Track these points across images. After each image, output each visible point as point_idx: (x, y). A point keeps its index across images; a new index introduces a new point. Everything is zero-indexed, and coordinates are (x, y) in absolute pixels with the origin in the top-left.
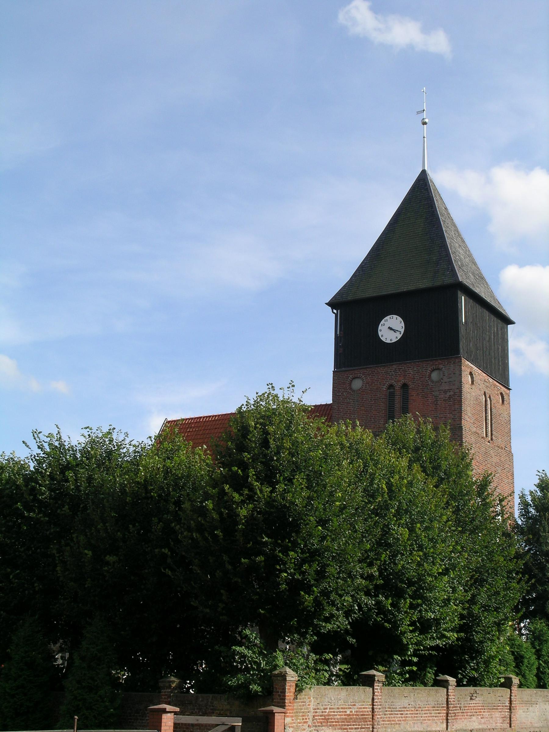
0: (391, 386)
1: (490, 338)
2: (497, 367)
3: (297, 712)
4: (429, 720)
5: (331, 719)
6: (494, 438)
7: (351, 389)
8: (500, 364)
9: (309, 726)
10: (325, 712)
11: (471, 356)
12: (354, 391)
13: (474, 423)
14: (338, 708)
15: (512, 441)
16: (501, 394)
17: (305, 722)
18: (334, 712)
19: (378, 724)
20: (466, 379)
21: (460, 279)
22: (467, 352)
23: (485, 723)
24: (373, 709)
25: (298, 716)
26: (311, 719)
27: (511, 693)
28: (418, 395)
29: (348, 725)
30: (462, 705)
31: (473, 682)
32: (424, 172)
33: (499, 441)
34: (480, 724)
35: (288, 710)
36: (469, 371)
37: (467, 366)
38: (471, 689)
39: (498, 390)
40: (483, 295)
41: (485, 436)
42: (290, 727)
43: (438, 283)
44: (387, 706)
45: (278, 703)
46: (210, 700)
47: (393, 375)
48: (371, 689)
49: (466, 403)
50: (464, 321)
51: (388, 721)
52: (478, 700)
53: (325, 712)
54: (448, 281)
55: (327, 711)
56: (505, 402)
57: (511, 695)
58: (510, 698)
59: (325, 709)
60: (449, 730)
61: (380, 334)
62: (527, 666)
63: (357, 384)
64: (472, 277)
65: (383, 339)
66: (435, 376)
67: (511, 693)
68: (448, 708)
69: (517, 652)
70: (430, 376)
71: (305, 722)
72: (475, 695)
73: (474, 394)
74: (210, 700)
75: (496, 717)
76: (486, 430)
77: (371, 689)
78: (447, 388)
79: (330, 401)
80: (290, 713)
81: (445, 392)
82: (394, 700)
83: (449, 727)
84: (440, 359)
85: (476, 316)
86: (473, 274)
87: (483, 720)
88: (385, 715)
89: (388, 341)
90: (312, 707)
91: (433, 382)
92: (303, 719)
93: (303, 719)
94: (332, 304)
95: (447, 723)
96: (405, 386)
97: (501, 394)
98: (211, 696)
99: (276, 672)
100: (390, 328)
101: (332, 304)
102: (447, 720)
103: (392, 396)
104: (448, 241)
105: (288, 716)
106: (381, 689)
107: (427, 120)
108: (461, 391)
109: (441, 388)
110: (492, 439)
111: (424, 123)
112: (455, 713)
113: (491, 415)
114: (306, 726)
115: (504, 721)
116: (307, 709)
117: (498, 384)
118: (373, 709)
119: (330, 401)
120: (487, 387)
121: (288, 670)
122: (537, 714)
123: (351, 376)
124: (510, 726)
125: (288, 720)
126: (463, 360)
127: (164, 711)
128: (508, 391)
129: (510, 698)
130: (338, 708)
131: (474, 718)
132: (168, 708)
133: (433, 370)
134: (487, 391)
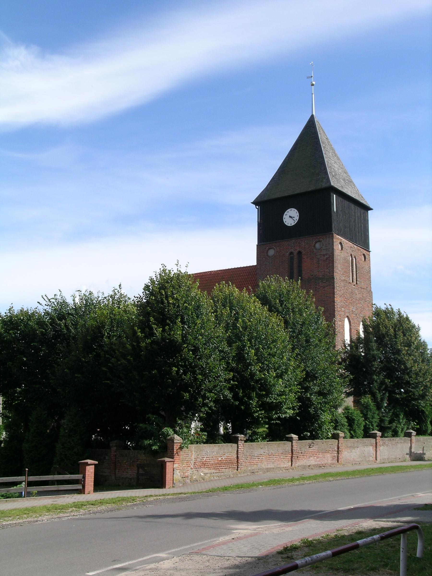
0: (291, 253)
1: (355, 220)
2: (361, 238)
3: (183, 461)
4: (279, 461)
5: (208, 463)
6: (358, 282)
7: (267, 255)
8: (363, 235)
9: (191, 468)
10: (203, 460)
11: (341, 232)
12: (269, 257)
13: (343, 274)
14: (213, 457)
15: (371, 284)
16: (364, 255)
17: (188, 466)
18: (209, 459)
19: (241, 465)
20: (337, 247)
21: (332, 184)
22: (337, 230)
23: (319, 461)
24: (237, 456)
25: (184, 463)
26: (193, 464)
27: (338, 442)
28: (307, 258)
29: (220, 467)
30: (303, 451)
31: (314, 437)
32: (312, 116)
33: (362, 284)
34: (315, 461)
35: (176, 459)
36: (339, 242)
37: (338, 239)
38: (310, 441)
39: (361, 252)
40: (349, 194)
41: (351, 281)
42: (177, 470)
43: (319, 187)
44: (248, 454)
45: (170, 455)
46: (136, 454)
47: (292, 246)
48: (236, 445)
49: (337, 262)
50: (335, 210)
51: (249, 463)
52: (315, 448)
53: (203, 460)
54: (324, 185)
55: (204, 459)
56: (366, 260)
57: (338, 444)
58: (338, 445)
59: (203, 458)
60: (293, 466)
61: (284, 220)
62: (357, 425)
63: (271, 252)
64: (343, 181)
65: (286, 224)
66: (318, 246)
67: (338, 442)
68: (292, 453)
69: (351, 417)
70: (314, 246)
71: (188, 466)
72: (312, 445)
73: (342, 256)
74: (136, 454)
75: (328, 457)
76: (352, 278)
77: (236, 445)
78: (325, 253)
79: (255, 263)
80: (177, 461)
81: (324, 255)
82: (253, 451)
83: (293, 465)
84: (275, 242)
85: (345, 207)
86: (344, 180)
87: (318, 459)
88: (247, 459)
89: (289, 225)
90: (193, 457)
91: (316, 249)
92: (187, 464)
93: (187, 464)
94: (256, 203)
95: (292, 462)
96: (300, 253)
97: (364, 255)
98: (136, 451)
99: (169, 438)
100: (290, 217)
101: (256, 203)
102: (292, 460)
103: (292, 259)
104: (326, 160)
105: (176, 463)
106: (243, 445)
107: (314, 83)
108: (333, 255)
109: (321, 253)
110: (357, 283)
111: (313, 85)
112: (298, 456)
113: (356, 268)
114: (189, 468)
115: (333, 459)
116: (190, 458)
117: (361, 249)
118: (237, 456)
119: (255, 263)
120: (353, 251)
121: (176, 436)
122: (358, 453)
123: (267, 248)
124: (338, 462)
125: (176, 466)
126: (335, 235)
127: (87, 464)
128: (368, 253)
129: (338, 445)
130: (213, 457)
131: (312, 458)
132: (89, 461)
133: (316, 243)
134: (352, 254)
